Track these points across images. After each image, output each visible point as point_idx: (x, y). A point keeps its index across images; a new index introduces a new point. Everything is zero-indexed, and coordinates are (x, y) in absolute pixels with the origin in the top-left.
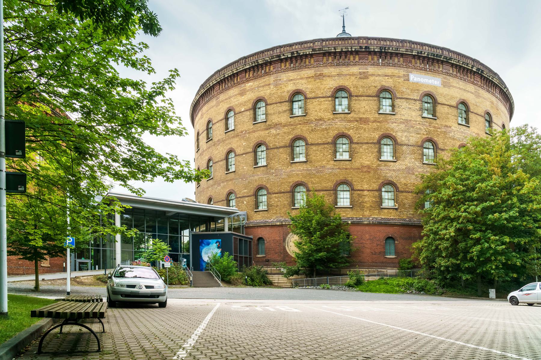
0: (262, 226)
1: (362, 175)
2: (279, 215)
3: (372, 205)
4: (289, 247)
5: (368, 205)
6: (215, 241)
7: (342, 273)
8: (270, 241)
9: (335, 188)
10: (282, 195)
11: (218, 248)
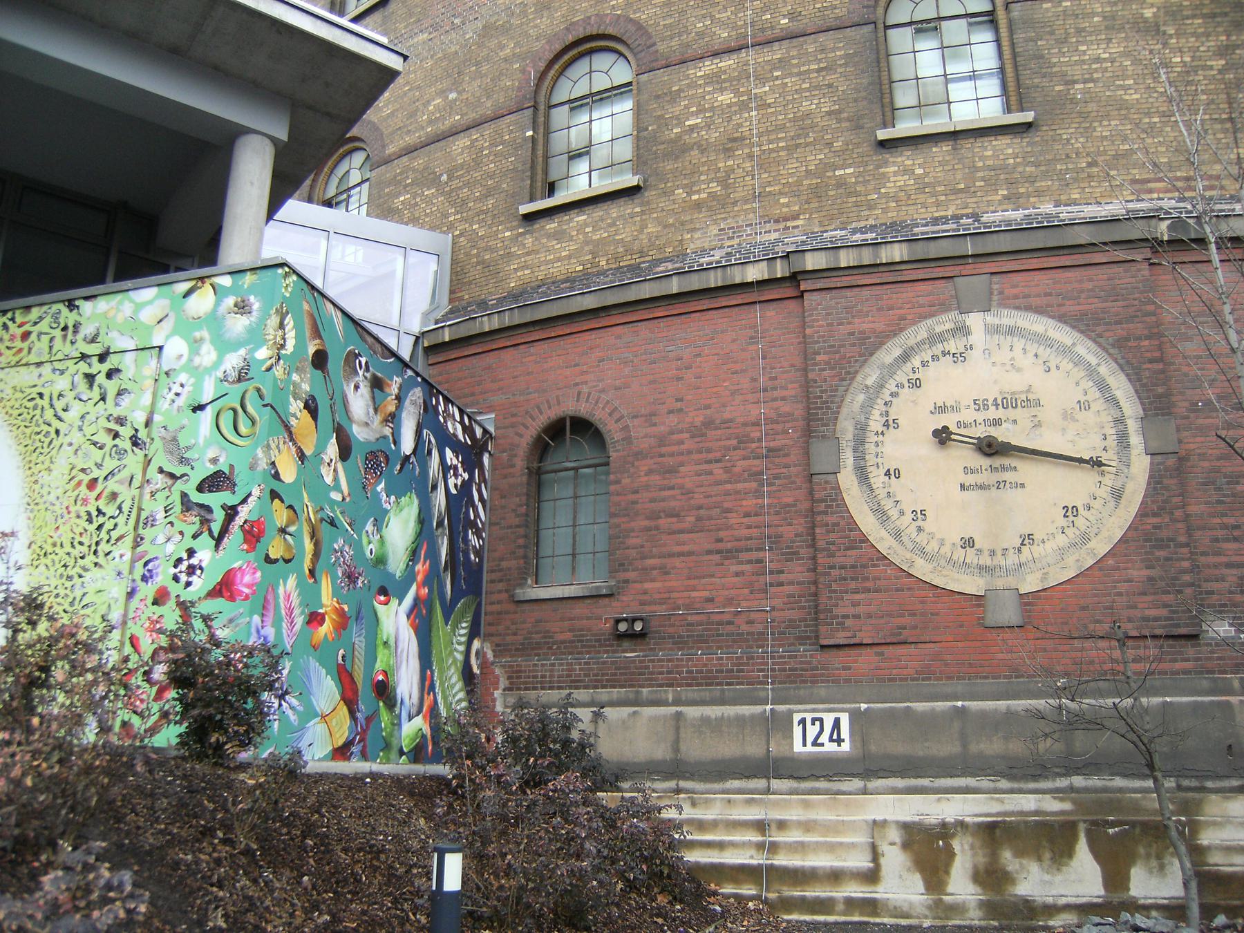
4: (877, 479)
8: (662, 440)
10: (777, 52)
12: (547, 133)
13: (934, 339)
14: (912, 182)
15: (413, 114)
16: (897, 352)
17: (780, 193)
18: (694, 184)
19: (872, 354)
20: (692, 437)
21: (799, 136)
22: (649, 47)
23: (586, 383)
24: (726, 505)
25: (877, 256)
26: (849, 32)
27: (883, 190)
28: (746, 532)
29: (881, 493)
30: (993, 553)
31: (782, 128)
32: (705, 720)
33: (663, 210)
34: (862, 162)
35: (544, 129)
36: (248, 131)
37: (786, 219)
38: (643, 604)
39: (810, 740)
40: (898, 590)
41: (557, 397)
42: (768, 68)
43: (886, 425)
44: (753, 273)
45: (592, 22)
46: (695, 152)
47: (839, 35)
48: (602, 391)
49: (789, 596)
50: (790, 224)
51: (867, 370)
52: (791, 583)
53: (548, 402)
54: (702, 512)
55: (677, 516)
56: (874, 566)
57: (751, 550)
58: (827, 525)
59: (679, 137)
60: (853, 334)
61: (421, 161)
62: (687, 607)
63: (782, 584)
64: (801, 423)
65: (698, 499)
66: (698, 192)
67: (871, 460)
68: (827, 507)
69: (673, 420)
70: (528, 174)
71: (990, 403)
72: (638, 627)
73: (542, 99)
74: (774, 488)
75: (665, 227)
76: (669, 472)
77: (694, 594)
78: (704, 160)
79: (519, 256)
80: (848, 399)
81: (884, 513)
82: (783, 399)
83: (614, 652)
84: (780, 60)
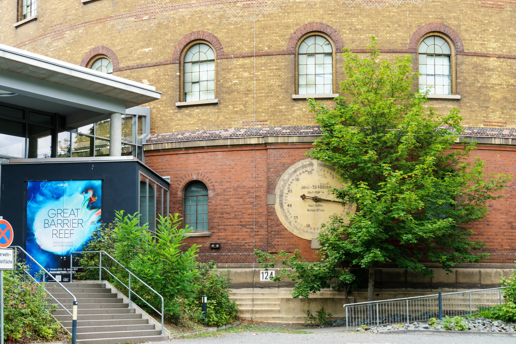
0: (203, 147)
1: (484, 15)
2: (253, 117)
3: (508, 96)
4: (285, 207)
5: (499, 96)
6: (81, 184)
7: (435, 280)
8: (224, 191)
9: (413, 45)
10: (263, 60)
11: (91, 206)
12: (184, 73)
13: (304, 166)
14: (302, 113)
15: (130, 53)
16: (293, 170)
17: (262, 112)
18: (235, 104)
19: (286, 170)
20: (234, 190)
21: (269, 93)
22: (221, 49)
23: (201, 170)
24: (243, 211)
26: (287, 56)
27: (293, 115)
28: (248, 220)
29: (286, 211)
30: (314, 229)
31: (264, 89)
32: (236, 273)
33: (225, 112)
34: (287, 104)
35: (182, 71)
36: (115, 113)
37: (263, 121)
38: (219, 239)
39: (264, 278)
40: (289, 238)
41: (191, 173)
42: (260, 65)
43: (289, 191)
44: (254, 141)
45: (200, 34)
46: (236, 93)
47: (283, 57)
48: (206, 173)
49: (260, 238)
50: (265, 123)
51: (284, 174)
52: (261, 235)
53: (188, 174)
54: (236, 213)
55: (229, 214)
56: (283, 231)
57: (250, 225)
58: (271, 219)
59: (231, 86)
60: (281, 163)
61: (135, 74)
62: (231, 241)
63: (258, 235)
64: (265, 189)
65: (235, 209)
66: (236, 108)
67: (284, 201)
68: (272, 214)
69: (228, 184)
70: (178, 90)
71: (317, 187)
72: (217, 246)
73: (182, 60)
74: (256, 207)
75: (226, 118)
76: (227, 200)
77: (233, 237)
78: (239, 96)
79: (176, 121)
80: (279, 183)
81: (286, 217)
82: (260, 181)
83: (210, 253)
84: (264, 63)
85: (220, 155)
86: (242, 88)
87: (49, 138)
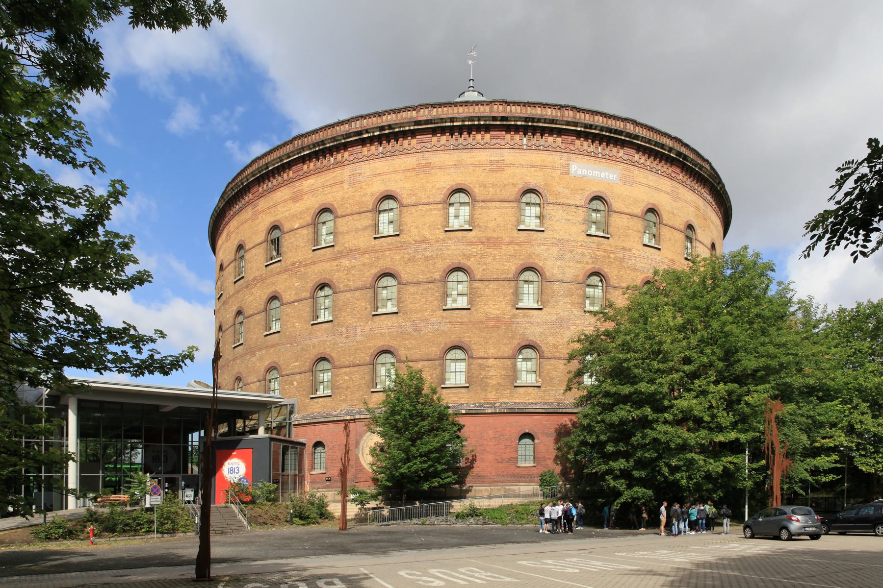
1: (487, 333)
3: (501, 382)
5: (494, 382)
9: (442, 355)
10: (356, 369)
25: (491, 110)
85: (331, 426)
86: (344, 386)
87: (197, 433)
